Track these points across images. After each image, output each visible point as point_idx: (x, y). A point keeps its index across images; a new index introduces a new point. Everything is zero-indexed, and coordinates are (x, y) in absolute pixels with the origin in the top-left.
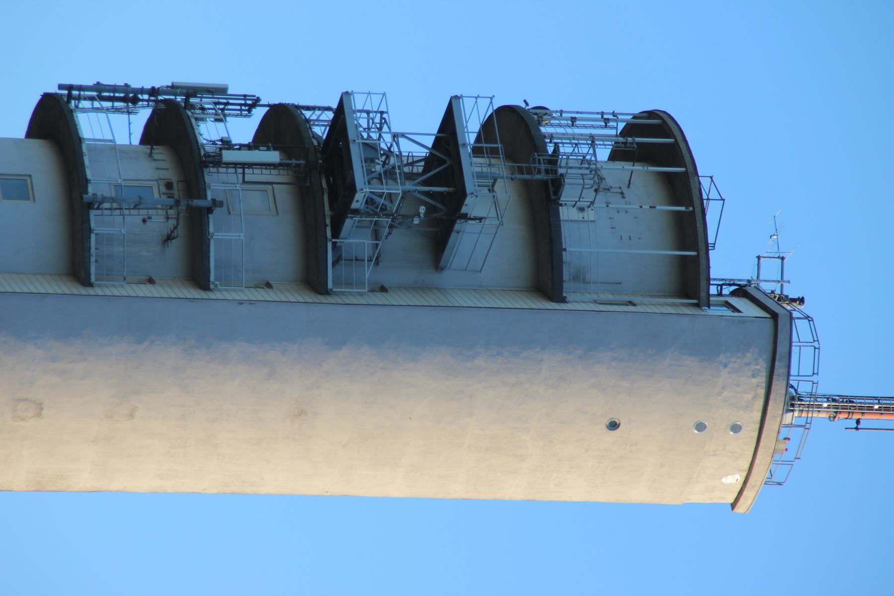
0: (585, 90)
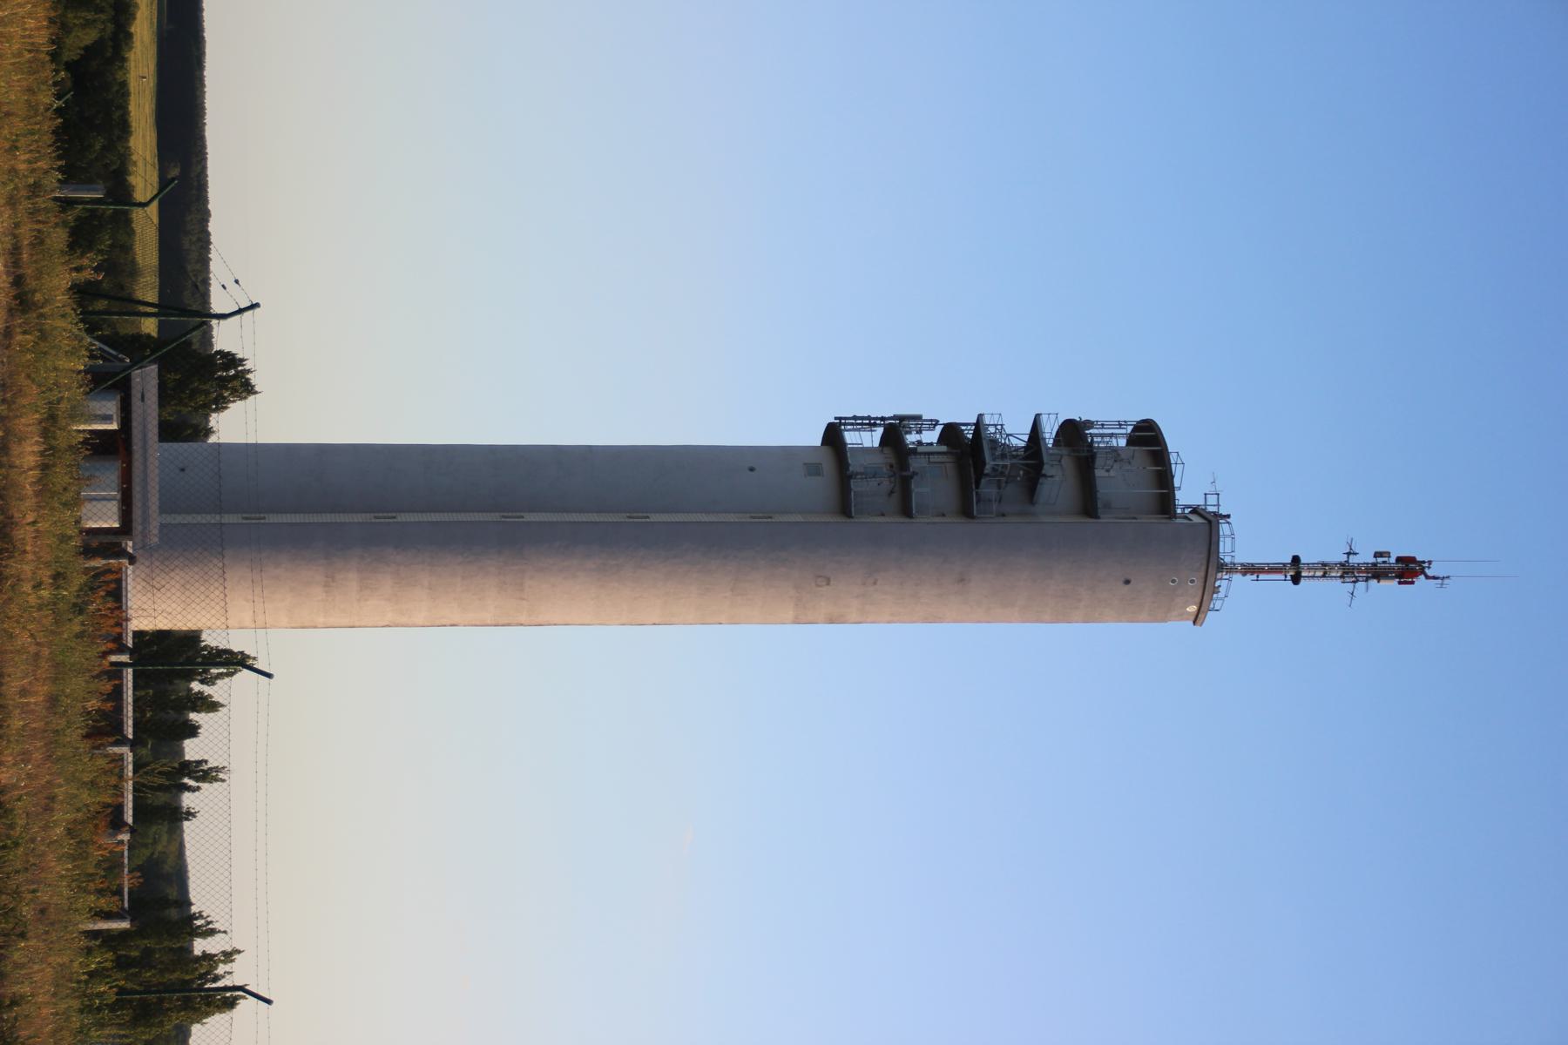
0: (1110, 408)
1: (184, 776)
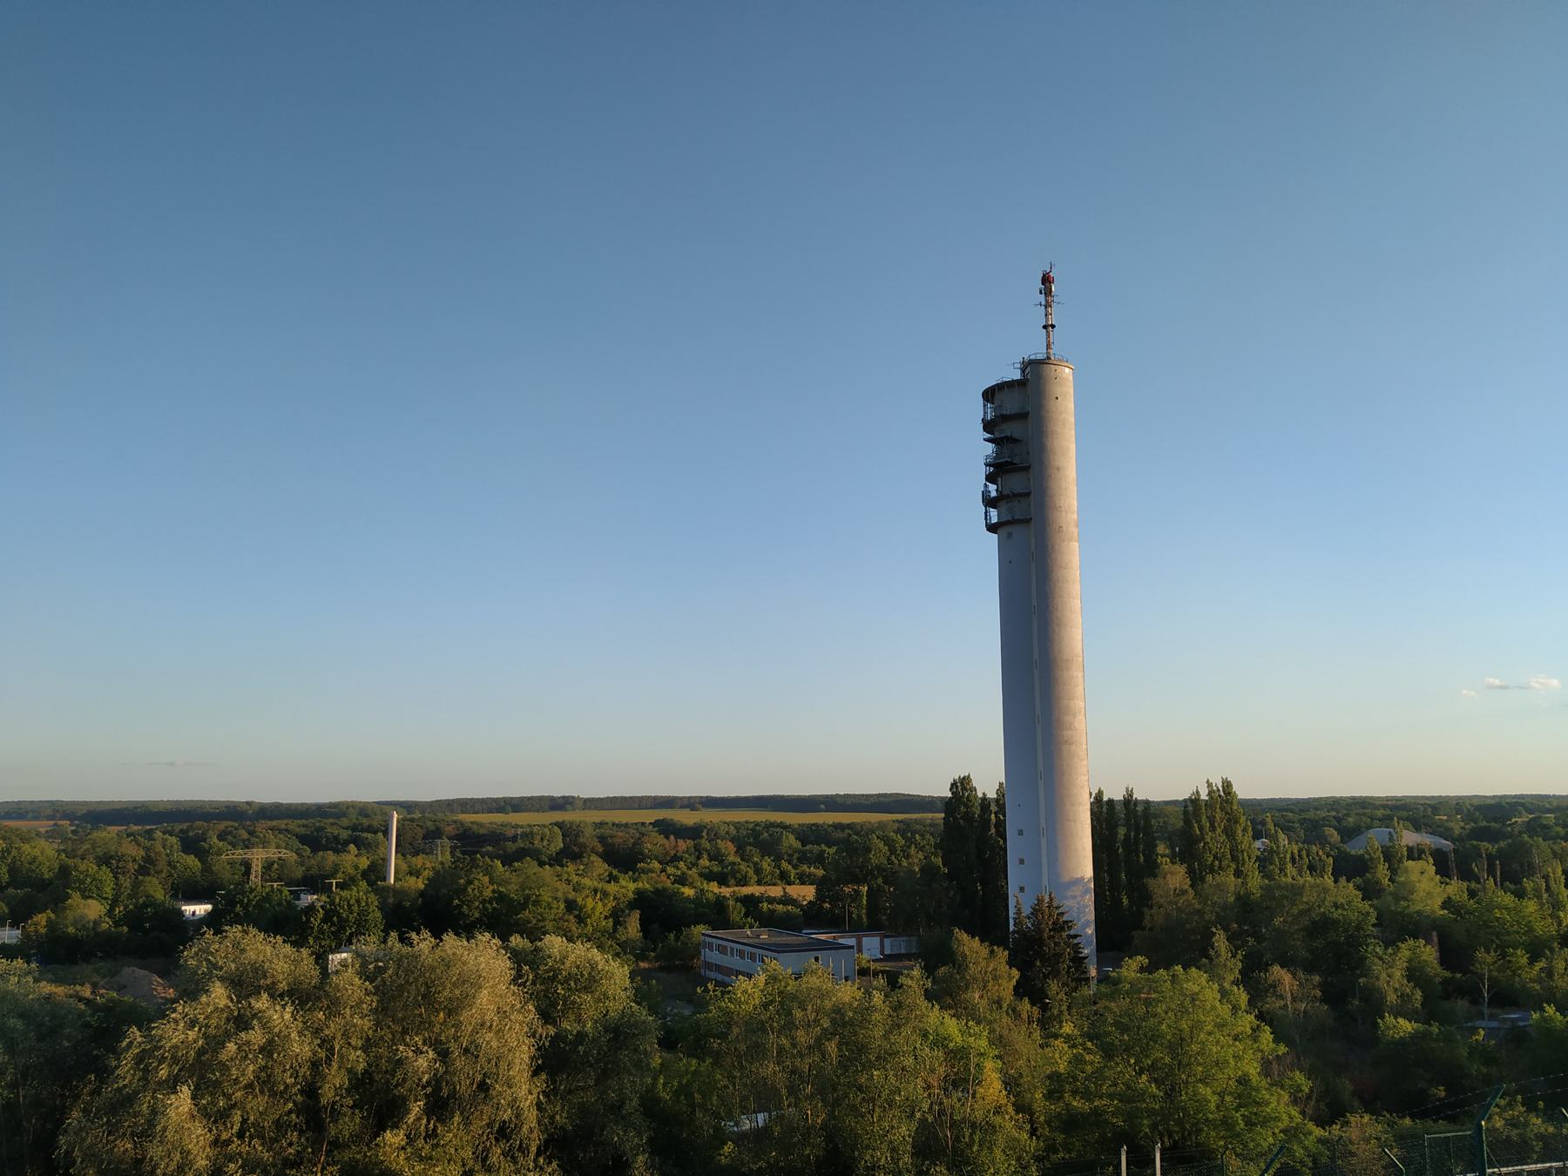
0: (976, 410)
1: (210, 914)
